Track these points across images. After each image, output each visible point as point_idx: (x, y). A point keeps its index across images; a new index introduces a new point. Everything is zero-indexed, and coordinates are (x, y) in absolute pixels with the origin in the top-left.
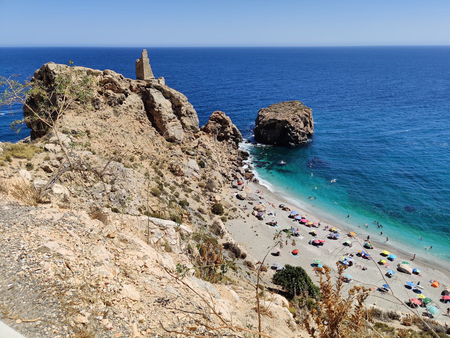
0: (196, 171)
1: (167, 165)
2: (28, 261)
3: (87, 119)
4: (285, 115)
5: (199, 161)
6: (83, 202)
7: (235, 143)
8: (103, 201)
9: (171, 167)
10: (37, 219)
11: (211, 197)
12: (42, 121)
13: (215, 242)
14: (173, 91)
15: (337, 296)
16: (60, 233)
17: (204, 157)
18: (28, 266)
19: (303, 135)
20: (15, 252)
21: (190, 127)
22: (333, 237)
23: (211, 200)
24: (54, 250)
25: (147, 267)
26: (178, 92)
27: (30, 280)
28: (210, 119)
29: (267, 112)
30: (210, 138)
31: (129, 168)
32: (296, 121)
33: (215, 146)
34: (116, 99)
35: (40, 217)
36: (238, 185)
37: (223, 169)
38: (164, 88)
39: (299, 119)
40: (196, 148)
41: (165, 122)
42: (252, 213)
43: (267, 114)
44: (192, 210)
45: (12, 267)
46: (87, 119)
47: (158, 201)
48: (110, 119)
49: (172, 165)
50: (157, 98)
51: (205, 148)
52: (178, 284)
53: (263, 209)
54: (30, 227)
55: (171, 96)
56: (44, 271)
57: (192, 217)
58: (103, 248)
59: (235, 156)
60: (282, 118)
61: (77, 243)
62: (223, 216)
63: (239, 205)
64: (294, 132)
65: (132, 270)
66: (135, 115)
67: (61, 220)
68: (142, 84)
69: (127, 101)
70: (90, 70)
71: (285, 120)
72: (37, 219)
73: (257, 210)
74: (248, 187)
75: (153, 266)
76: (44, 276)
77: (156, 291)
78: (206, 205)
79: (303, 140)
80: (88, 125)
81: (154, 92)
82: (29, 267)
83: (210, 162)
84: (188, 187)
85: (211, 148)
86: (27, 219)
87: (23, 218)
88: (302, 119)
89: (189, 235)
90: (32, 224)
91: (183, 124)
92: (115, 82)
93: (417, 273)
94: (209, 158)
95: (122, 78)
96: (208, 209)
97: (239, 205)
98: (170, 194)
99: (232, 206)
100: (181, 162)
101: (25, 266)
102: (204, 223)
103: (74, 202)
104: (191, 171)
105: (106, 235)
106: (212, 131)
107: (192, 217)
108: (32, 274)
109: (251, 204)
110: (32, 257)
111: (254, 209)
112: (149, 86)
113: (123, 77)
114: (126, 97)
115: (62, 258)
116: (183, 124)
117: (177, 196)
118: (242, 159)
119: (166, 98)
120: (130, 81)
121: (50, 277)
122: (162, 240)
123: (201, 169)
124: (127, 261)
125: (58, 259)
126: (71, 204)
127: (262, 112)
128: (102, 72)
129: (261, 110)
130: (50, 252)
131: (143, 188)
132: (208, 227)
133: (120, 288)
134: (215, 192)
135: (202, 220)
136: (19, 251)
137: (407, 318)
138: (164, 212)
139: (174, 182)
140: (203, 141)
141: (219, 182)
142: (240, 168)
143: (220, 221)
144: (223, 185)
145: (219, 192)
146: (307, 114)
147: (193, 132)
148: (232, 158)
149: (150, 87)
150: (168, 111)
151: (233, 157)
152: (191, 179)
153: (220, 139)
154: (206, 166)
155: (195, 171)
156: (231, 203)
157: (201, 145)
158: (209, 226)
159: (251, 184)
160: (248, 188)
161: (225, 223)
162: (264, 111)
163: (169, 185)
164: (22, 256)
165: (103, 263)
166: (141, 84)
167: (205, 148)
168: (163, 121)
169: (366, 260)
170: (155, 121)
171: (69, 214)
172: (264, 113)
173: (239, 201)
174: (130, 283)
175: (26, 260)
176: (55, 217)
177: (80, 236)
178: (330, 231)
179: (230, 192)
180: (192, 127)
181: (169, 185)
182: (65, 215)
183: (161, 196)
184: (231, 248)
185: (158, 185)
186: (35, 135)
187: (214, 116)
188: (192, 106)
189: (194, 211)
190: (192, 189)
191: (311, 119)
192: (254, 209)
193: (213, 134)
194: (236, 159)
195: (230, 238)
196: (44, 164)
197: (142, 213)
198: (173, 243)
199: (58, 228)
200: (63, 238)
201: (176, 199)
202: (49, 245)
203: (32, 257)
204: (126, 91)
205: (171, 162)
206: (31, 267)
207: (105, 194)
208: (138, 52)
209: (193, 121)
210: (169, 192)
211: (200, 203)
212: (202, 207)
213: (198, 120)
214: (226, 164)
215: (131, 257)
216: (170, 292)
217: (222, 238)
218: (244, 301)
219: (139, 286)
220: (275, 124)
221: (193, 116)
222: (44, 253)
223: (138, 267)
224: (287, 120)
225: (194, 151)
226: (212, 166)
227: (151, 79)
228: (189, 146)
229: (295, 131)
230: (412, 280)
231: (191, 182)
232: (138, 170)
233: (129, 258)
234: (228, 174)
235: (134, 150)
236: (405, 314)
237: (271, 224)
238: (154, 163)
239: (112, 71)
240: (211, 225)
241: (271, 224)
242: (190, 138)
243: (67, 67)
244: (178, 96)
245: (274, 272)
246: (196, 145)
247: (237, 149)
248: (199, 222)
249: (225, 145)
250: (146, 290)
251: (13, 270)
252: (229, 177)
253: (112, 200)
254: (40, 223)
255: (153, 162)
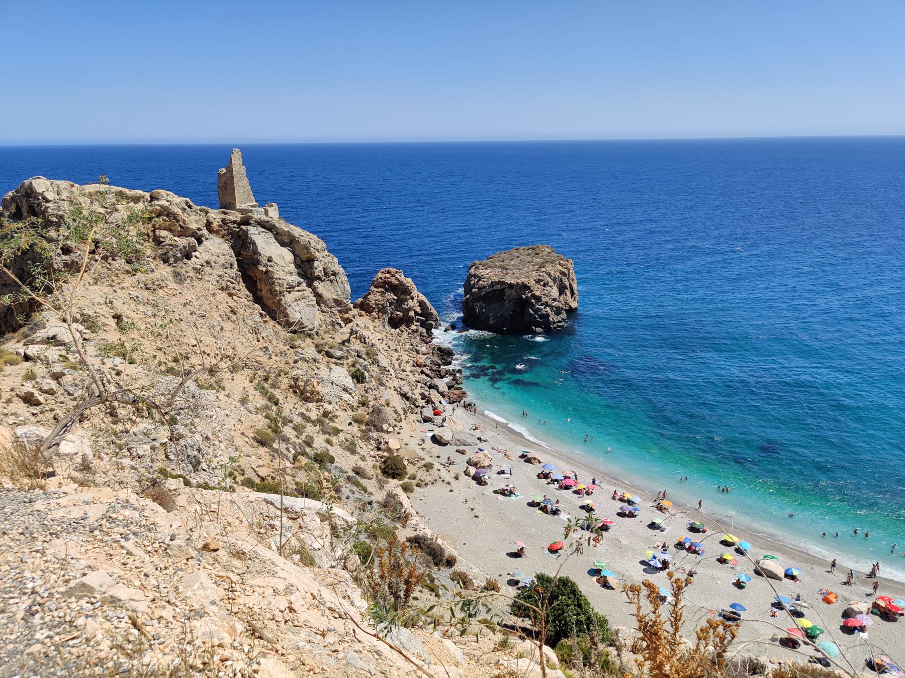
0: (347, 391)
1: (285, 381)
2: (47, 619)
3: (115, 291)
4: (521, 274)
5: (353, 369)
6: (123, 468)
7: (424, 330)
8: (152, 461)
9: (296, 384)
10: (52, 520)
11: (381, 443)
12: (38, 301)
13: (391, 535)
14: (297, 231)
15: (673, 643)
16: (106, 548)
17: (362, 360)
18: (50, 630)
19: (558, 311)
20: (16, 600)
21: (332, 301)
22: (627, 513)
23: (379, 449)
24: (103, 590)
25: (295, 611)
26: (306, 233)
27: (58, 664)
28: (373, 284)
29: (486, 269)
30: (373, 321)
31: (207, 388)
32: (544, 285)
33: (385, 338)
34: (178, 249)
35: (58, 514)
36: (435, 415)
37: (402, 385)
38: (277, 225)
39: (550, 280)
40: (346, 344)
41: (281, 292)
42: (465, 472)
43: (487, 271)
44: (342, 471)
45: (13, 637)
46: (115, 291)
47: (270, 455)
48: (165, 289)
49: (297, 380)
50: (264, 245)
51: (365, 343)
52: (359, 642)
53: (486, 463)
54: (41, 538)
55: (291, 241)
56: (88, 640)
57: (341, 486)
58: (203, 576)
59: (426, 356)
60: (516, 280)
61: (145, 571)
62: (406, 480)
63: (438, 457)
64: (540, 307)
65: (266, 621)
66: (217, 281)
67: (105, 520)
68: (231, 218)
69: (202, 251)
70: (121, 191)
71: (523, 282)
72: (52, 520)
73: (475, 465)
74: (454, 419)
75: (306, 606)
76: (89, 652)
77: (326, 667)
78: (369, 459)
79: (560, 322)
80: (117, 303)
81: (257, 232)
82: (51, 633)
83: (374, 369)
84: (330, 424)
85: (378, 343)
86: (31, 520)
87: (22, 519)
88: (554, 280)
89: (351, 527)
90: (44, 533)
91: (318, 296)
92: (176, 214)
93: (793, 578)
94: (373, 363)
95: (190, 207)
96: (374, 467)
97: (438, 457)
98: (294, 439)
99: (423, 459)
100: (316, 374)
101: (42, 631)
102: (366, 498)
103: (105, 470)
104: (336, 390)
105: (200, 545)
106: (378, 308)
107: (341, 486)
108: (61, 649)
109: (462, 452)
110: (56, 610)
111: (469, 462)
112: (246, 222)
113: (191, 204)
114: (199, 244)
115: (121, 607)
116: (318, 296)
117: (309, 444)
118: (440, 362)
119: (283, 244)
120: (207, 212)
121: (102, 655)
122: (294, 542)
123: (357, 385)
124: (253, 601)
125: (113, 609)
126: (98, 475)
127: (477, 268)
128: (147, 195)
129: (475, 264)
130: (95, 595)
131: (238, 430)
132: (375, 505)
133: (255, 667)
134: (388, 432)
135: (363, 492)
136: (25, 598)
137: (781, 669)
138: (282, 479)
139: (302, 415)
140: (359, 329)
141: (396, 412)
142: (437, 381)
143: (399, 491)
144: (403, 417)
145: (396, 433)
146: (564, 270)
147: (339, 311)
148: (421, 361)
149: (249, 224)
150: (286, 270)
151: (422, 359)
152: (338, 408)
153: (394, 323)
154: (367, 380)
155: (345, 390)
156: (421, 453)
157: (356, 338)
158: (378, 502)
159: (460, 411)
160: (455, 420)
161: (411, 495)
162: (481, 267)
163: (291, 421)
164: (34, 608)
165: (206, 610)
166: (231, 217)
167: (365, 343)
168: (276, 291)
169: (694, 555)
170: (261, 290)
171: (119, 505)
172: (481, 271)
173: (436, 449)
174: (267, 651)
175: (42, 618)
176: (90, 514)
177: (149, 552)
178: (621, 500)
179: (418, 430)
180: (336, 301)
181: (291, 421)
182: (111, 508)
183: (275, 446)
184: (424, 547)
185: (269, 422)
186: (3, 328)
187: (381, 278)
188: (336, 260)
189: (346, 473)
190: (340, 428)
191: (573, 280)
192: (467, 462)
193: (380, 314)
194: (428, 362)
195: (422, 526)
196: (24, 388)
197: (236, 483)
198: (317, 546)
199: (99, 537)
200: (114, 559)
201: (308, 450)
202: (91, 579)
203: (56, 610)
204: (200, 233)
205: (295, 373)
206: (58, 634)
207: (157, 445)
208: (222, 155)
209: (338, 290)
210: (291, 437)
211: (357, 457)
212: (361, 464)
213: (348, 288)
214: (408, 373)
215: (260, 591)
216: (355, 667)
217: (404, 527)
218: (471, 662)
219: (288, 657)
220: (502, 291)
221: (338, 279)
222: (80, 598)
223: (277, 612)
224: (526, 283)
225: (341, 350)
226: (380, 380)
227: (250, 208)
228: (331, 340)
229: (542, 305)
230: (786, 591)
231: (338, 413)
232: (226, 393)
233: (256, 594)
234: (413, 394)
235: (217, 352)
236: (776, 661)
237: (503, 492)
238: (260, 377)
239: (169, 193)
240: (381, 500)
241: (503, 492)
242: (333, 324)
243: (72, 186)
244: (307, 239)
245: (512, 592)
246: (346, 337)
247: (430, 342)
248: (357, 495)
249: (405, 335)
250: (304, 664)
251: (17, 642)
252: (416, 399)
253: (172, 457)
254: (59, 529)
255: (257, 376)
